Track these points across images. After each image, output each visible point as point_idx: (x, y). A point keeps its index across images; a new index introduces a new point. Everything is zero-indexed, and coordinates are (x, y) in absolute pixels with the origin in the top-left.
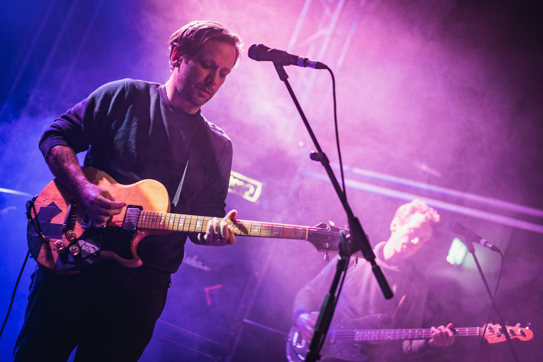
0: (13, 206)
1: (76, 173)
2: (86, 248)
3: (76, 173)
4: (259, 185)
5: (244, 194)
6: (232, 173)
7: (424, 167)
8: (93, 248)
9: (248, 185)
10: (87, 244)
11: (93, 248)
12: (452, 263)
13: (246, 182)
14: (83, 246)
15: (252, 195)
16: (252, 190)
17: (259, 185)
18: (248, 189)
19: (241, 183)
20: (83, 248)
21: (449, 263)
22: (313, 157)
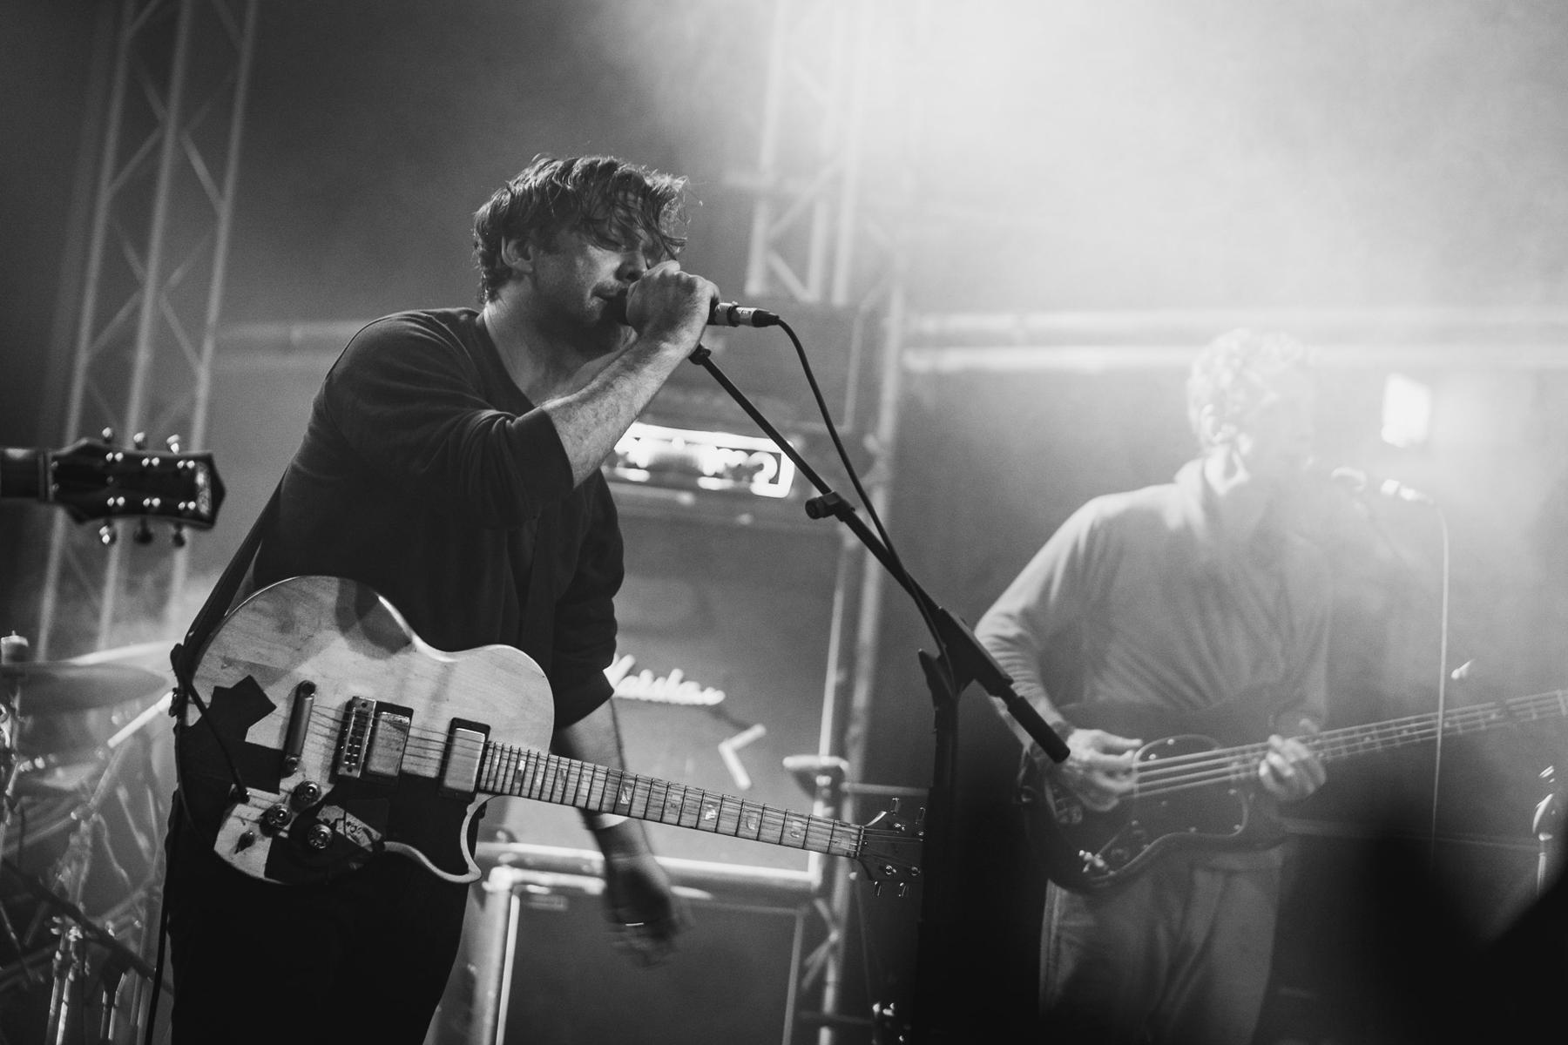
2: (348, 829)
10: (350, 818)
11: (366, 831)
14: (341, 824)
15: (774, 481)
19: (739, 459)
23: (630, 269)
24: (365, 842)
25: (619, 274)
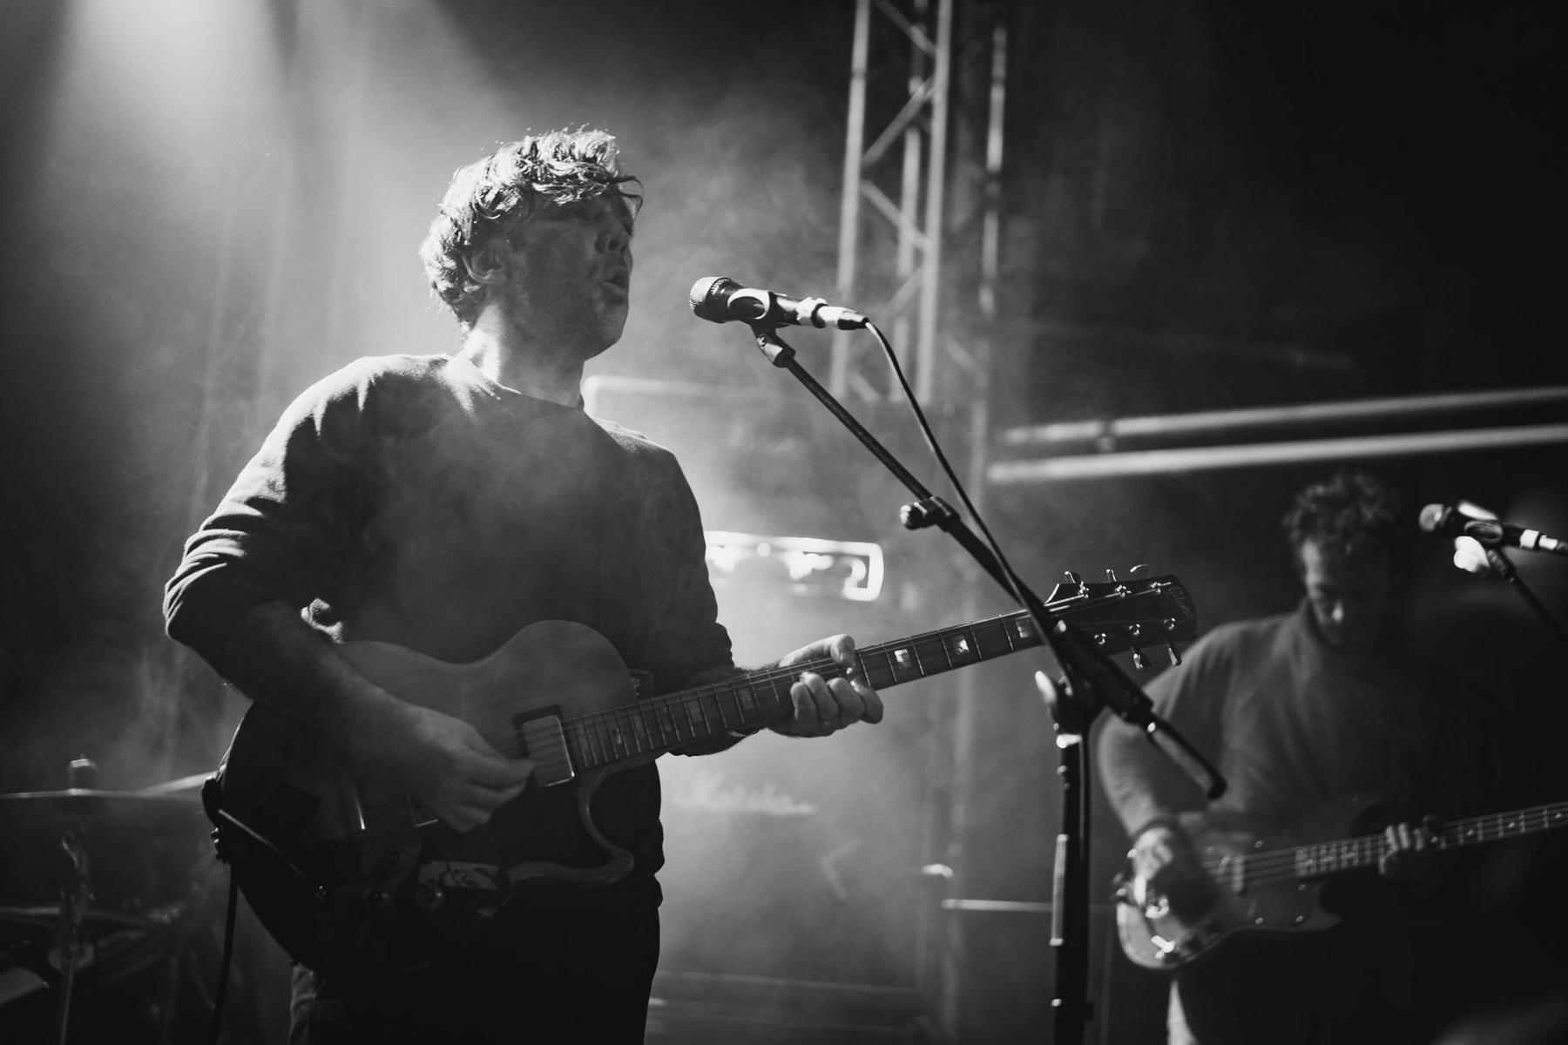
0: (299, 955)
1: (308, 133)
2: (458, 878)
3: (308, 133)
4: (874, 551)
5: (841, 586)
6: (710, 537)
7: (1299, 358)
8: (478, 870)
9: (845, 561)
10: (454, 866)
11: (478, 870)
12: (1471, 568)
13: (837, 556)
14: (448, 877)
15: (863, 584)
16: (858, 569)
17: (874, 551)
18: (849, 571)
20: (450, 882)
21: (1464, 571)
22: (916, 520)
23: (609, 238)
24: (485, 883)
25: (599, 247)
